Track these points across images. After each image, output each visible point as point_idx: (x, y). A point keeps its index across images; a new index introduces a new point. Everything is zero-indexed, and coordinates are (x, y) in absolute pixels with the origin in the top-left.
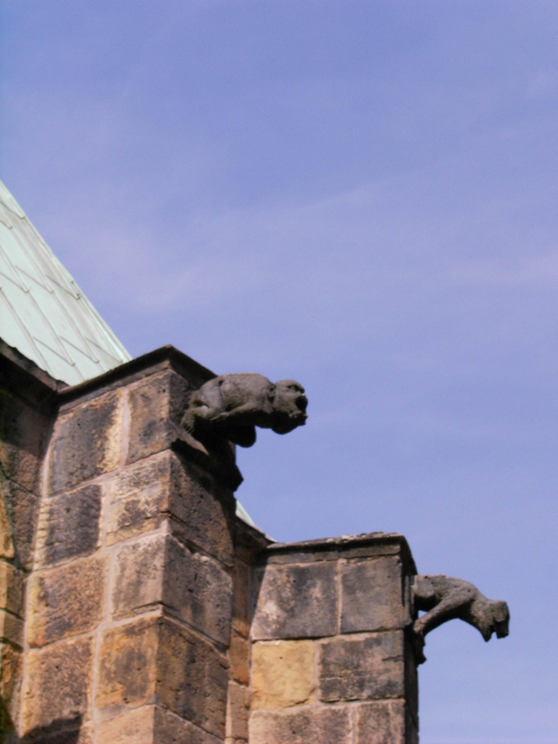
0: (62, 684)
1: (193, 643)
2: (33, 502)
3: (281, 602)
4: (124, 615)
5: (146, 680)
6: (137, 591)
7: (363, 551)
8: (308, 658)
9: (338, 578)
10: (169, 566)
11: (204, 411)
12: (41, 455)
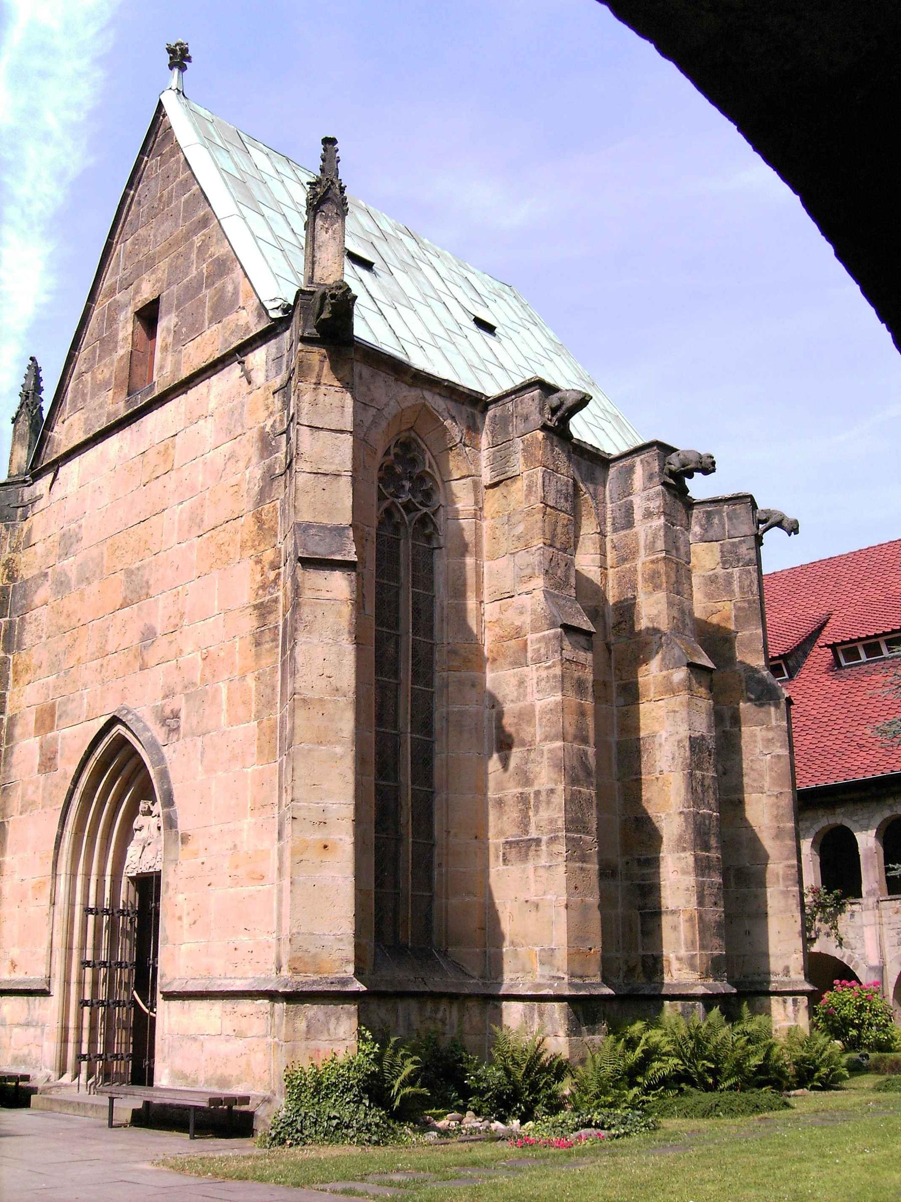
0: (626, 583)
1: (677, 564)
2: (604, 507)
3: (701, 526)
4: (649, 555)
5: (661, 582)
6: (654, 546)
7: (736, 501)
8: (715, 550)
9: (725, 514)
10: (665, 536)
11: (673, 467)
12: (605, 487)
